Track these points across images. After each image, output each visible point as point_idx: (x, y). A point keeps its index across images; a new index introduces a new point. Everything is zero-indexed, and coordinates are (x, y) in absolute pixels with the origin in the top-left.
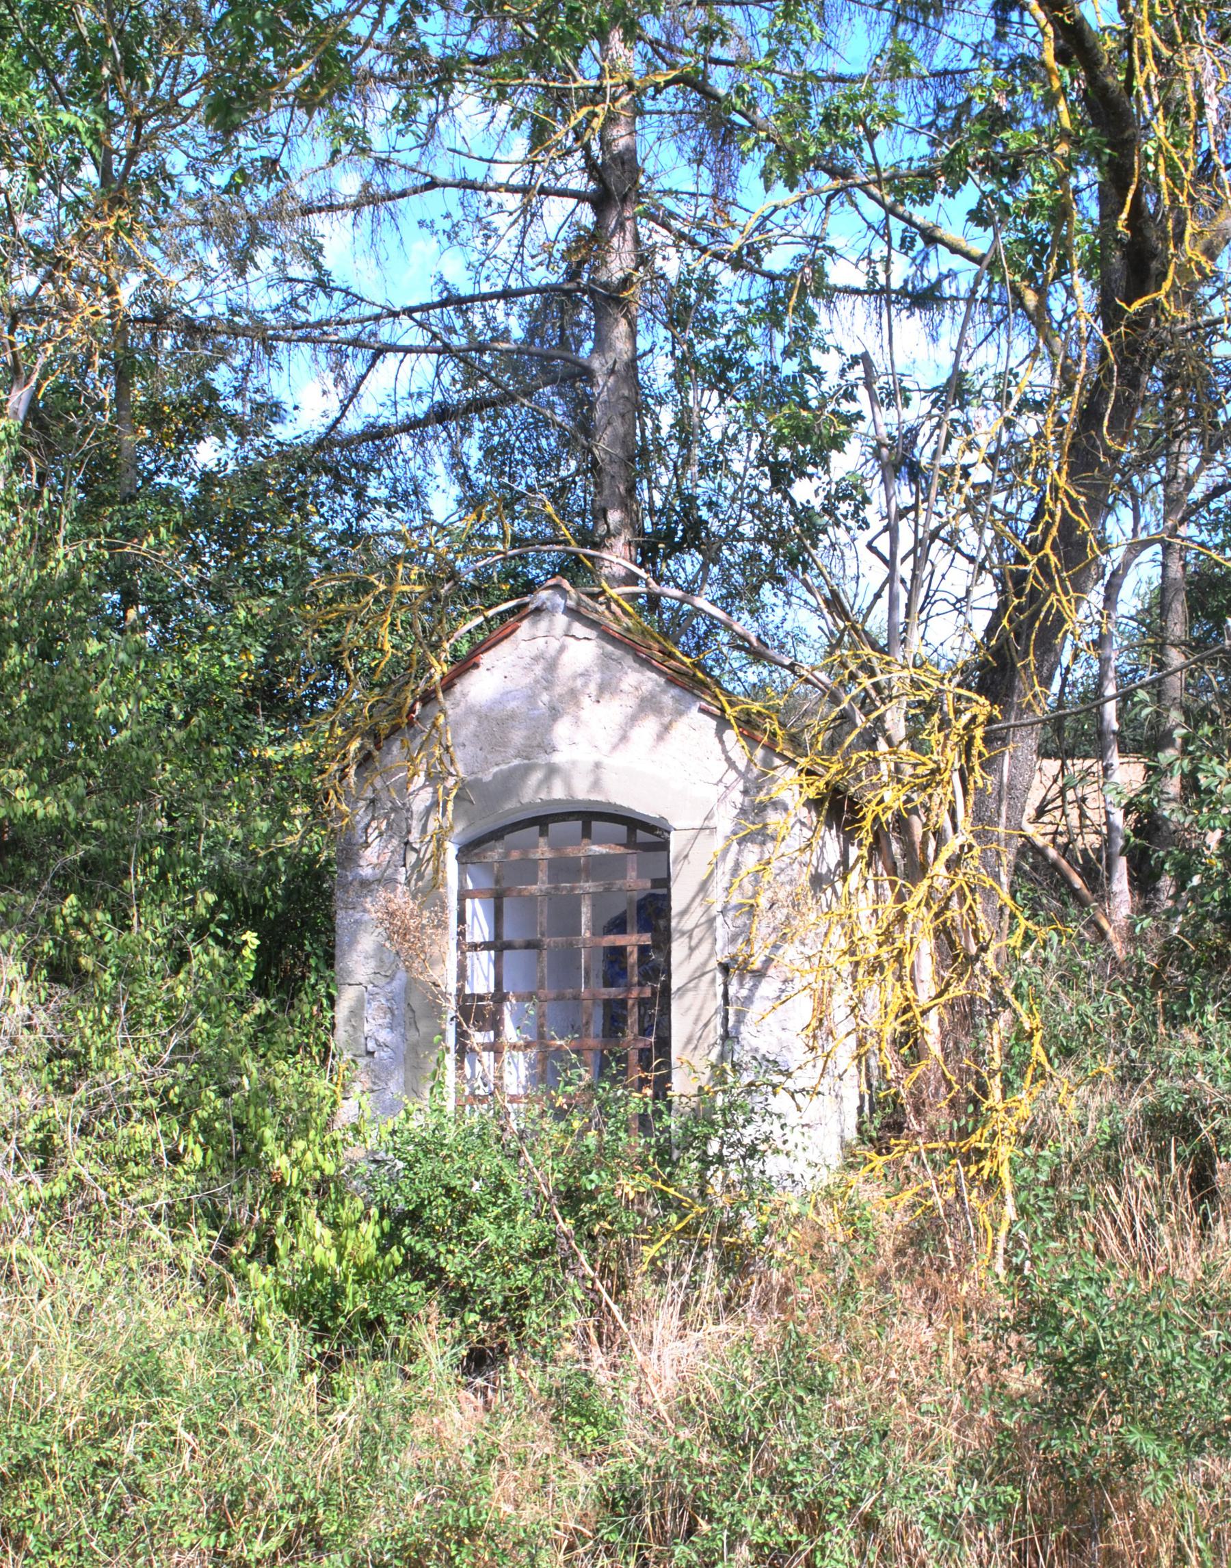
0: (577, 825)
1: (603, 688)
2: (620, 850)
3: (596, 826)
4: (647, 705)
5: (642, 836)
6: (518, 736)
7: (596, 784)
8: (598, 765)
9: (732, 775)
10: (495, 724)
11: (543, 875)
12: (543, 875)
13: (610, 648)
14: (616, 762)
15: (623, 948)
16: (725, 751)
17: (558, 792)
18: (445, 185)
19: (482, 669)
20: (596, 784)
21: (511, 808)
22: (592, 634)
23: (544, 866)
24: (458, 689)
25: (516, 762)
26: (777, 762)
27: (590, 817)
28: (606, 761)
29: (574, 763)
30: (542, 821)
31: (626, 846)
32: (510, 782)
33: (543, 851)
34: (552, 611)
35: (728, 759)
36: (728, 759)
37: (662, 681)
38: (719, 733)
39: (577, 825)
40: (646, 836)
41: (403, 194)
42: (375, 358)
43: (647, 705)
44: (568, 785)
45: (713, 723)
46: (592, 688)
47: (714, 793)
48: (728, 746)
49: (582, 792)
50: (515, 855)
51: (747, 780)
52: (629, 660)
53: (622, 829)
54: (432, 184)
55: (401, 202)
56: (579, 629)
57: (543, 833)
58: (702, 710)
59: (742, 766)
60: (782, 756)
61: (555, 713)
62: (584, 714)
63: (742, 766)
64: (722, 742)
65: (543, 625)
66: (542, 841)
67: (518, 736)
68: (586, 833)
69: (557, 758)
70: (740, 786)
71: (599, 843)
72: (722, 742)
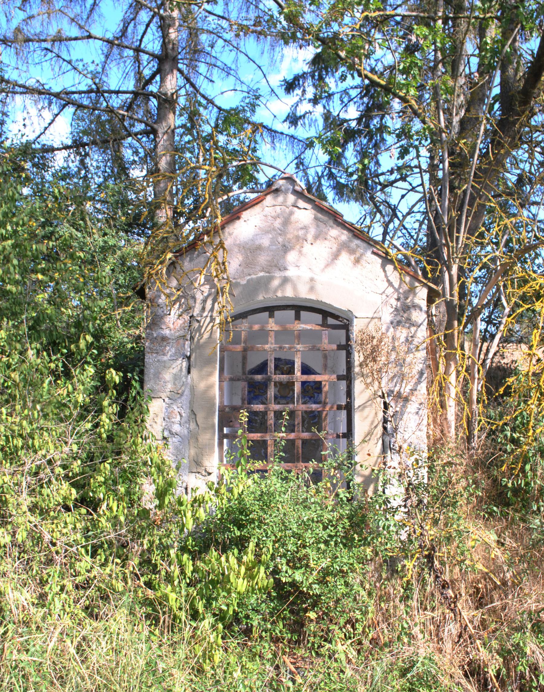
0: (292, 313)
1: (316, 237)
2: (318, 328)
3: (303, 313)
4: (344, 246)
5: (331, 321)
6: (263, 259)
7: (312, 289)
8: (312, 280)
9: (391, 290)
10: (251, 250)
11: (271, 339)
12: (271, 339)
13: (320, 215)
14: (322, 278)
15: (320, 383)
16: (386, 276)
17: (289, 292)
18: (95, 38)
19: (241, 220)
20: (312, 289)
21: (262, 298)
22: (308, 206)
23: (272, 334)
24: (227, 230)
25: (262, 274)
26: (417, 284)
27: (299, 308)
28: (316, 277)
29: (299, 277)
30: (271, 310)
31: (322, 326)
32: (263, 284)
33: (272, 325)
34: (286, 192)
35: (388, 281)
36: (388, 281)
37: (350, 235)
38: (383, 266)
39: (292, 313)
40: (336, 320)
41: (76, 39)
42: (64, 106)
43: (344, 246)
44: (295, 288)
45: (380, 261)
46: (310, 237)
47: (379, 299)
48: (388, 274)
49: (304, 293)
50: (256, 327)
51: (399, 293)
52: (331, 222)
53: (319, 317)
54: (90, 37)
55: (73, 43)
56: (301, 203)
57: (271, 316)
58: (374, 253)
59: (396, 285)
60: (420, 282)
61: (286, 249)
62: (304, 250)
63: (396, 285)
64: (385, 271)
65: (281, 199)
66: (271, 320)
67: (263, 259)
68: (298, 317)
69: (288, 273)
70: (396, 296)
71: (305, 323)
72: (385, 271)
